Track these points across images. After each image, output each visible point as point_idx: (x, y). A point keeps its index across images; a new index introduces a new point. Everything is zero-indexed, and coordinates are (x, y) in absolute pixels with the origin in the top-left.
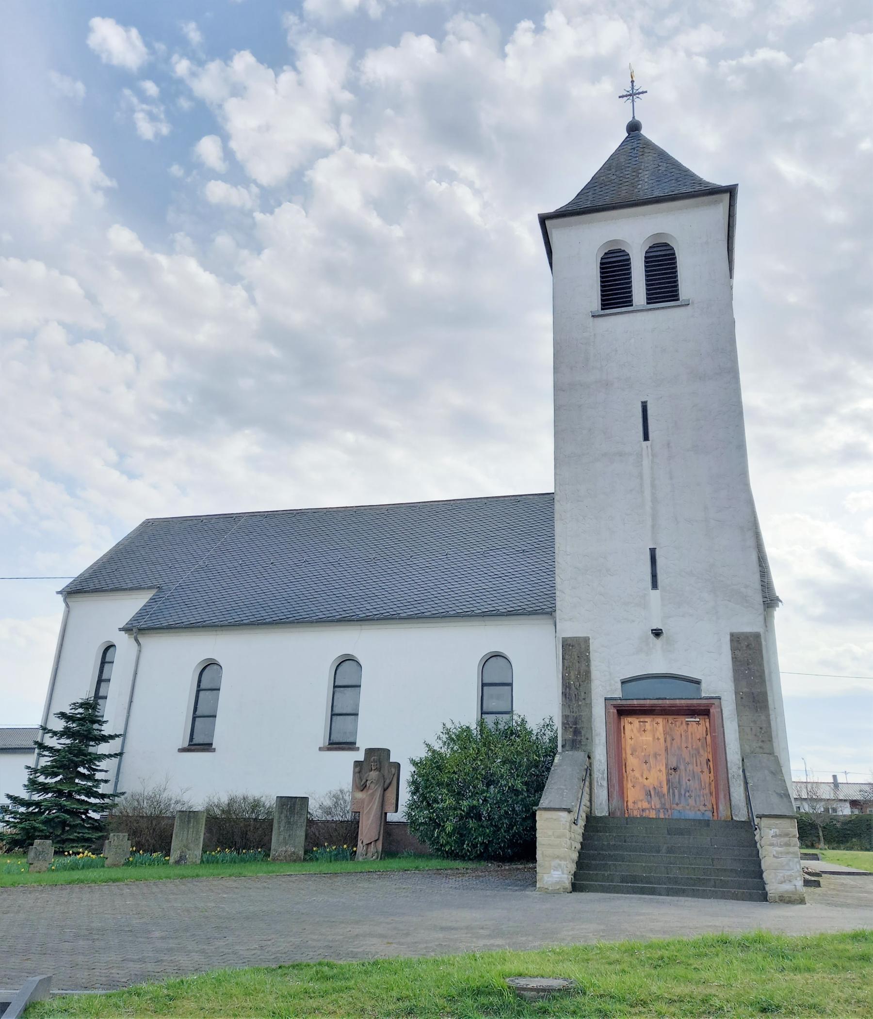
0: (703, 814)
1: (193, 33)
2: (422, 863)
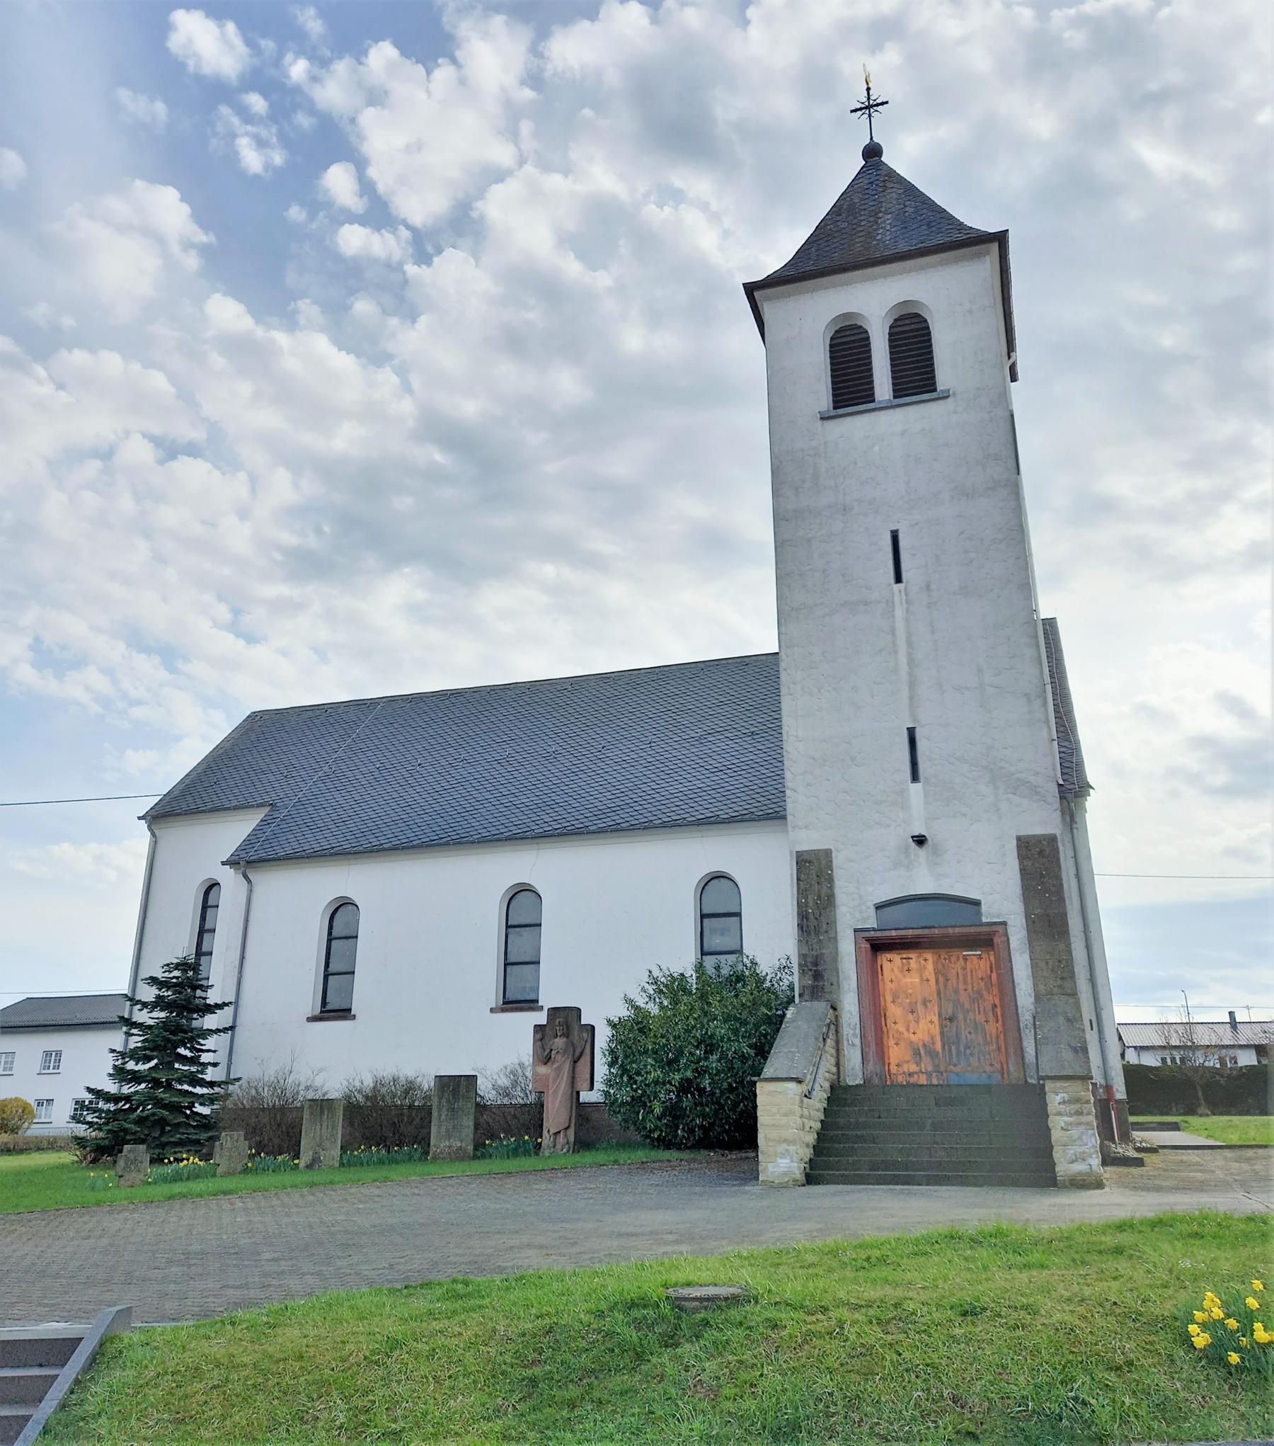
0: (990, 1076)
1: (312, 23)
2: (623, 1156)
